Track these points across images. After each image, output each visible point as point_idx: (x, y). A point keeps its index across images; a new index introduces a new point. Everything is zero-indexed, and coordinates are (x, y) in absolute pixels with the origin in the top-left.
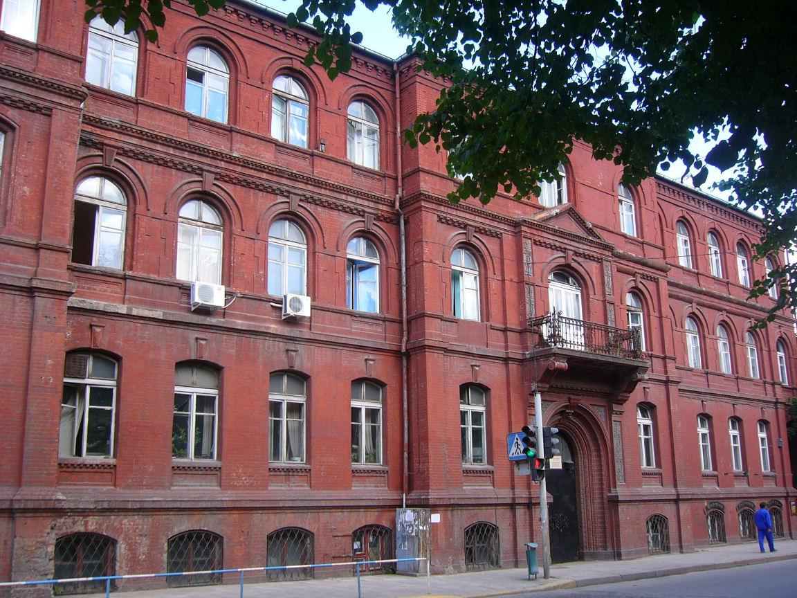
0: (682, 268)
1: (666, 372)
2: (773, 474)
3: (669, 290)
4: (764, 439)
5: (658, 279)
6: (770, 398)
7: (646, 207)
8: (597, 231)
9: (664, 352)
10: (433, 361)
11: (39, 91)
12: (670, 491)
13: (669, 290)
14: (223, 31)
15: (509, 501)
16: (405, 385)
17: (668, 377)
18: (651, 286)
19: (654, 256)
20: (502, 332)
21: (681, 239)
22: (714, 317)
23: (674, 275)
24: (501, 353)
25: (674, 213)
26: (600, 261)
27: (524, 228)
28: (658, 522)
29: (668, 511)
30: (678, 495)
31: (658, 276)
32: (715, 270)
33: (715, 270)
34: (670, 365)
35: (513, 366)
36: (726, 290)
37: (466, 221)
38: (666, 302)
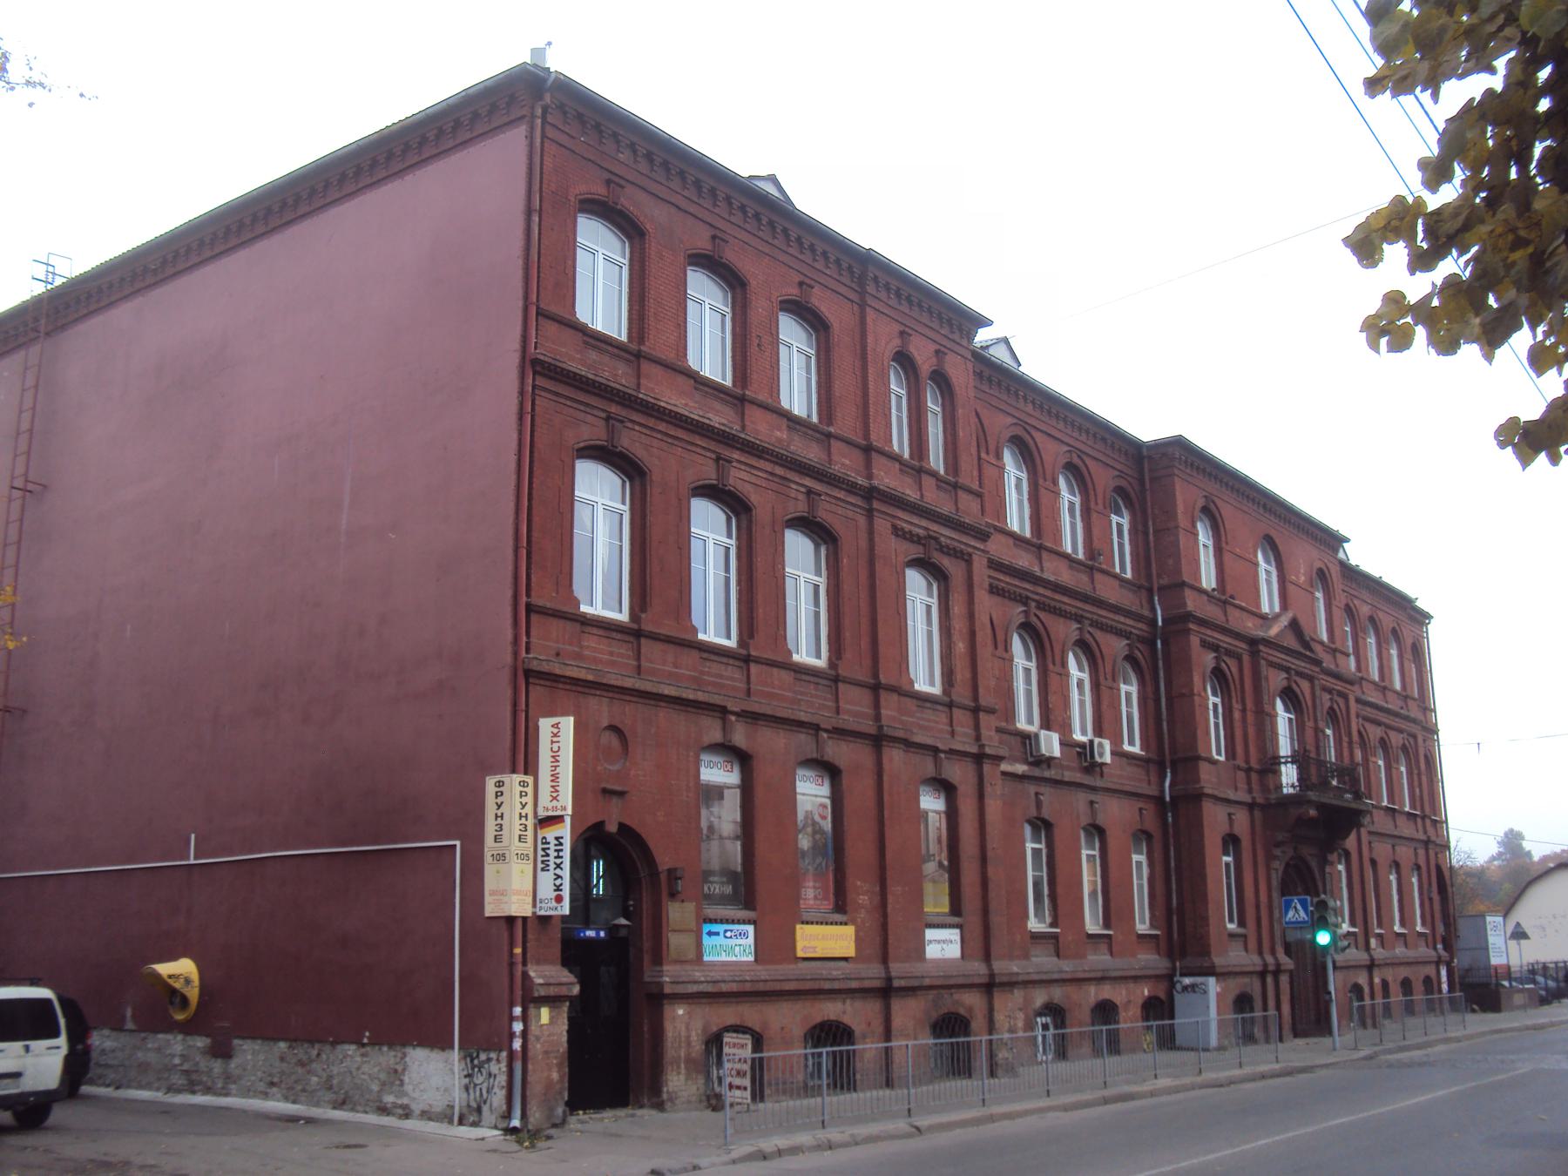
0: (1012, 535)
1: (978, 738)
2: (1241, 931)
3: (990, 577)
4: (1141, 862)
5: (970, 555)
6: (1422, 836)
7: (1228, 548)
8: (1313, 644)
9: (1247, 761)
10: (1208, 807)
11: (721, 446)
12: (1362, 957)
13: (990, 577)
14: (1028, 427)
15: (877, 984)
16: (1171, 841)
17: (880, 728)
18: (1305, 685)
19: (969, 509)
20: (968, 713)
21: (1013, 473)
22: (1063, 631)
23: (998, 547)
24: (1247, 798)
25: (1000, 424)
26: (1311, 679)
27: (1261, 648)
28: (950, 1025)
29: (1362, 980)
30: (889, 979)
31: (970, 550)
32: (1071, 538)
33: (1071, 538)
34: (988, 722)
35: (1257, 813)
36: (1381, 696)
37: (899, 522)
38: (985, 602)
